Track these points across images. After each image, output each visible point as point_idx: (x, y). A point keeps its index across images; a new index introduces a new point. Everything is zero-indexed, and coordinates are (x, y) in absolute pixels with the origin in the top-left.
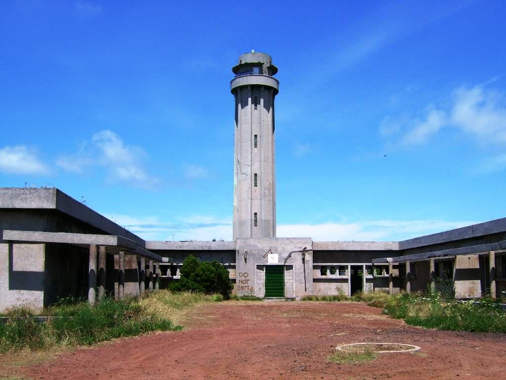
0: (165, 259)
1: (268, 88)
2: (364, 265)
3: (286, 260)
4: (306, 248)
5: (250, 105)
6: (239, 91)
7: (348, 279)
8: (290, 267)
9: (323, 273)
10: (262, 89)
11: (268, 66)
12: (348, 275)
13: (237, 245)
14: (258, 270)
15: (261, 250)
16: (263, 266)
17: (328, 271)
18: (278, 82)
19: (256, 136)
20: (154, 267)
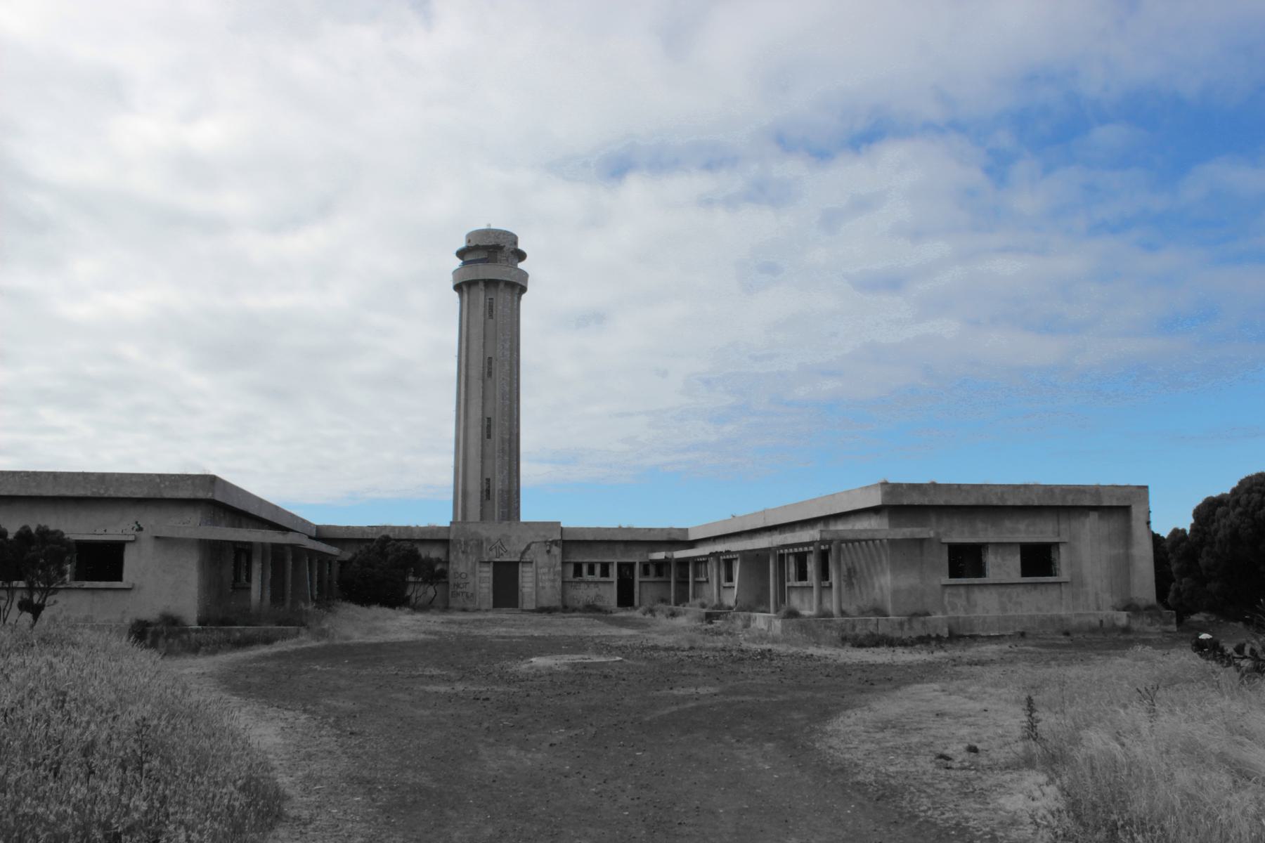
3: (523, 553)
6: (465, 288)
10: (502, 286)
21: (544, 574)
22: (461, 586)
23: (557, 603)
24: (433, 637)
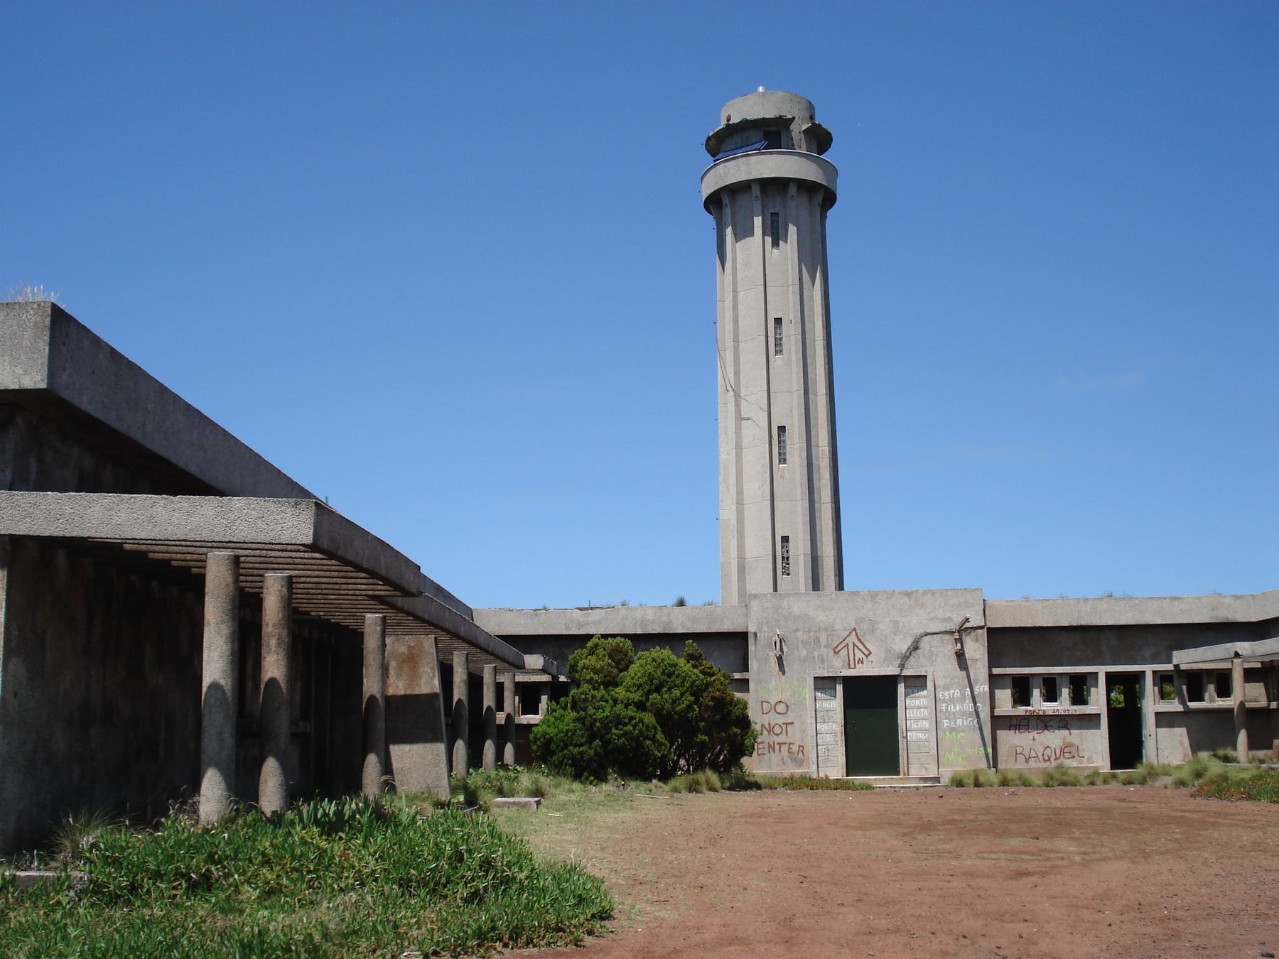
0: (534, 661)
1: (805, 186)
2: (1148, 669)
3: (905, 658)
4: (967, 620)
6: (726, 200)
7: (1099, 715)
8: (918, 682)
9: (1022, 696)
10: (792, 190)
11: (805, 127)
12: (1098, 701)
14: (819, 694)
15: (826, 630)
16: (833, 680)
17: (1036, 694)
18: (831, 170)
19: (778, 321)
20: (499, 688)
21: (952, 701)
22: (777, 730)
23: (782, 746)
24: (804, 268)
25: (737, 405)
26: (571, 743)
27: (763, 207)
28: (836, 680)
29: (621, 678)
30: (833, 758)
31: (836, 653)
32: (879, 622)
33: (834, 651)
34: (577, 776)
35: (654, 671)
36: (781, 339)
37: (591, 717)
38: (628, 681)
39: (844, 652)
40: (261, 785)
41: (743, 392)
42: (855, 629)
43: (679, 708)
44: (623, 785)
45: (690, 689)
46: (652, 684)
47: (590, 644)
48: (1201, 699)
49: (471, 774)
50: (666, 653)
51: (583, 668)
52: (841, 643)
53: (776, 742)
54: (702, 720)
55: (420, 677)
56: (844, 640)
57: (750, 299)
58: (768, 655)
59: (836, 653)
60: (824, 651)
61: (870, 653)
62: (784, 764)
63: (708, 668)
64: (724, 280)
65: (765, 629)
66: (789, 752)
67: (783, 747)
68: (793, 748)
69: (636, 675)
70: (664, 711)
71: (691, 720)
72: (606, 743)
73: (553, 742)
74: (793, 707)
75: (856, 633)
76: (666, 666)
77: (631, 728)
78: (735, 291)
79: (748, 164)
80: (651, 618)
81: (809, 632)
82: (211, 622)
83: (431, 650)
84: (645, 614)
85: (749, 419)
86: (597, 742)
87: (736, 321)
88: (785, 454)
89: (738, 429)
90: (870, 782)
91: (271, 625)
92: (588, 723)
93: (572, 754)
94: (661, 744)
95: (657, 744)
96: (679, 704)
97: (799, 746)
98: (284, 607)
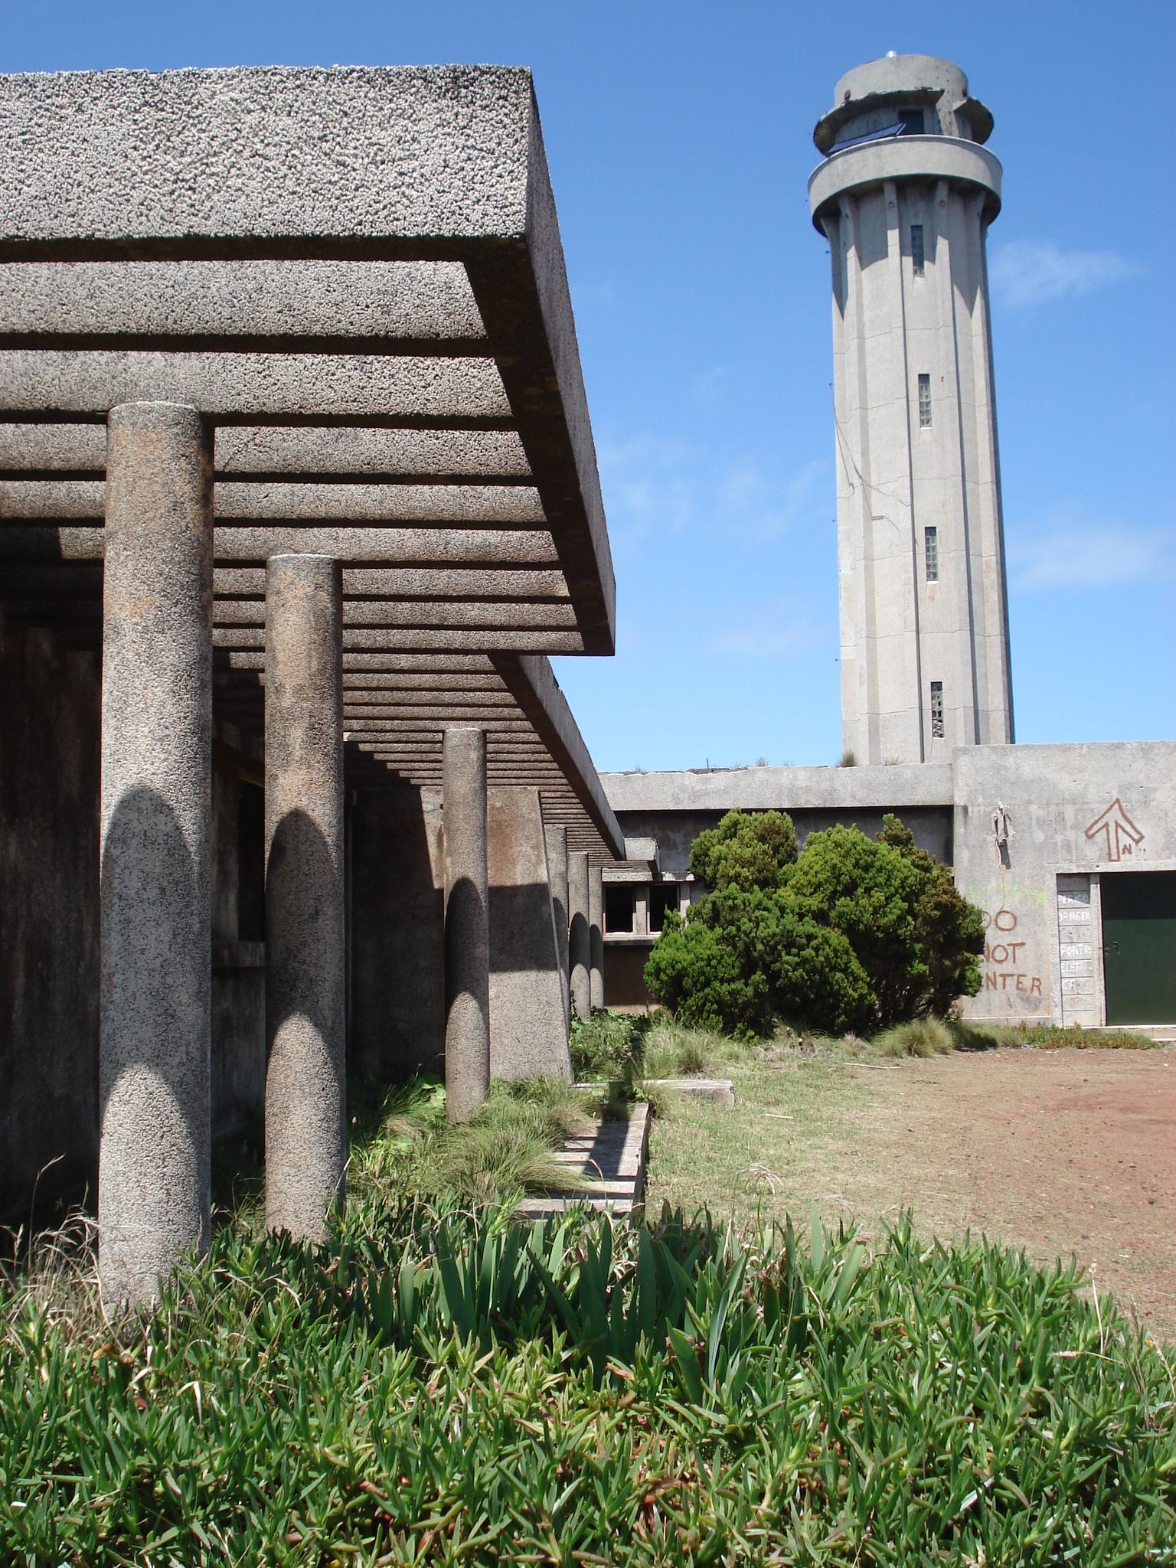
0: (641, 848)
1: (962, 189)
5: (894, 261)
6: (846, 209)
10: (942, 192)
13: (961, 781)
14: (1063, 899)
15: (1073, 802)
16: (1087, 877)
18: (995, 166)
19: (924, 378)
25: (866, 499)
26: (716, 978)
27: (901, 219)
28: (1089, 879)
29: (784, 873)
30: (1084, 997)
31: (1090, 837)
32: (1154, 790)
33: (1087, 835)
34: (727, 1030)
35: (841, 862)
36: (928, 404)
37: (747, 934)
38: (798, 878)
39: (1101, 836)
40: (270, 1120)
41: (874, 481)
42: (1118, 801)
43: (883, 921)
44: (800, 1044)
45: (900, 891)
46: (839, 882)
47: (724, 821)
48: (628, 928)
49: (575, 1031)
50: (849, 834)
51: (719, 859)
52: (1096, 822)
53: (998, 974)
54: (917, 940)
55: (514, 863)
56: (1102, 817)
57: (883, 349)
58: (985, 840)
59: (1090, 837)
60: (1071, 835)
61: (1142, 837)
62: (1011, 1006)
63: (921, 859)
64: (843, 330)
65: (980, 800)
66: (1018, 988)
67: (1009, 981)
68: (1024, 982)
69: (811, 868)
70: (861, 926)
71: (905, 939)
72: (773, 977)
73: (687, 975)
74: (1024, 920)
75: (1120, 806)
76: (860, 854)
77: (814, 953)
78: (861, 337)
79: (879, 157)
80: (804, 785)
81: (1048, 805)
82: (126, 626)
83: (533, 814)
84: (795, 778)
85: (881, 518)
86: (758, 976)
87: (863, 380)
88: (935, 566)
89: (868, 531)
90: (1146, 1035)
91: (288, 688)
92: (740, 945)
93: (719, 994)
94: (856, 979)
95: (851, 979)
96: (885, 915)
97: (1034, 979)
98: (324, 639)
